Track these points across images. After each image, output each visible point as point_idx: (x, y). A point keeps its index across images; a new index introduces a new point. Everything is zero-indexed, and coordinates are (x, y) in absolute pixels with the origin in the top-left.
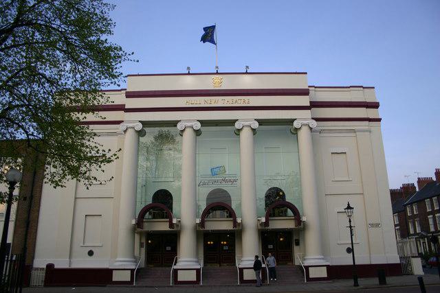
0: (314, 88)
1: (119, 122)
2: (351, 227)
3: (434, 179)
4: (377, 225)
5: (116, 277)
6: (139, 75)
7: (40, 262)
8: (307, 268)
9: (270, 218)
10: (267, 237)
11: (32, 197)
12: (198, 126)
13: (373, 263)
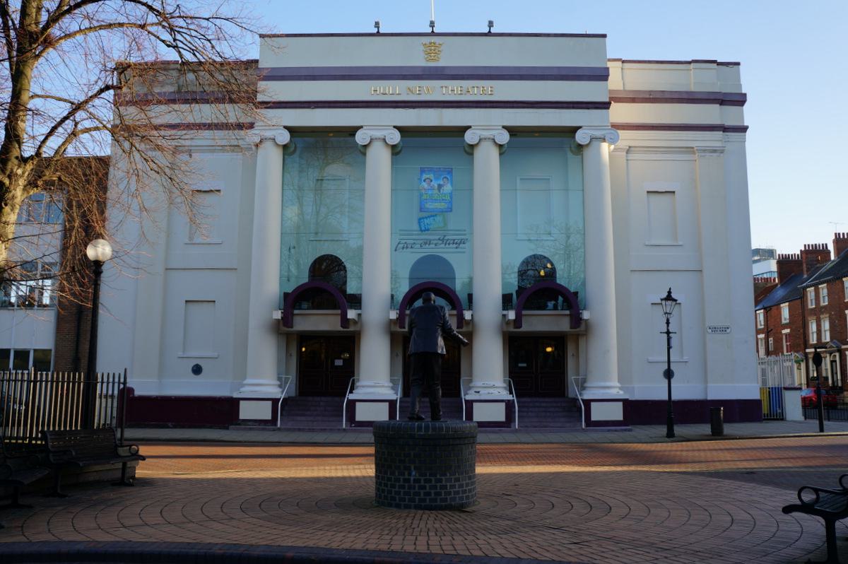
2: (668, 333)
4: (724, 330)
8: (588, 403)
9: (524, 312)
12: (396, 138)
13: (710, 397)
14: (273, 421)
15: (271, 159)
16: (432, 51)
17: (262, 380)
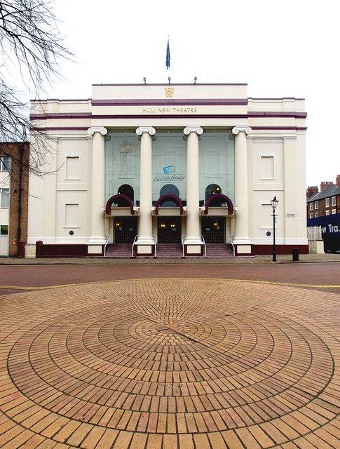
0: (251, 100)
1: (86, 129)
2: (274, 216)
3: (335, 183)
4: (293, 215)
5: (91, 250)
6: (103, 85)
7: (32, 239)
8: (236, 246)
10: (205, 222)
11: (21, 190)
12: (153, 132)
14: (103, 254)
15: (99, 142)
16: (169, 93)
17: (97, 237)
